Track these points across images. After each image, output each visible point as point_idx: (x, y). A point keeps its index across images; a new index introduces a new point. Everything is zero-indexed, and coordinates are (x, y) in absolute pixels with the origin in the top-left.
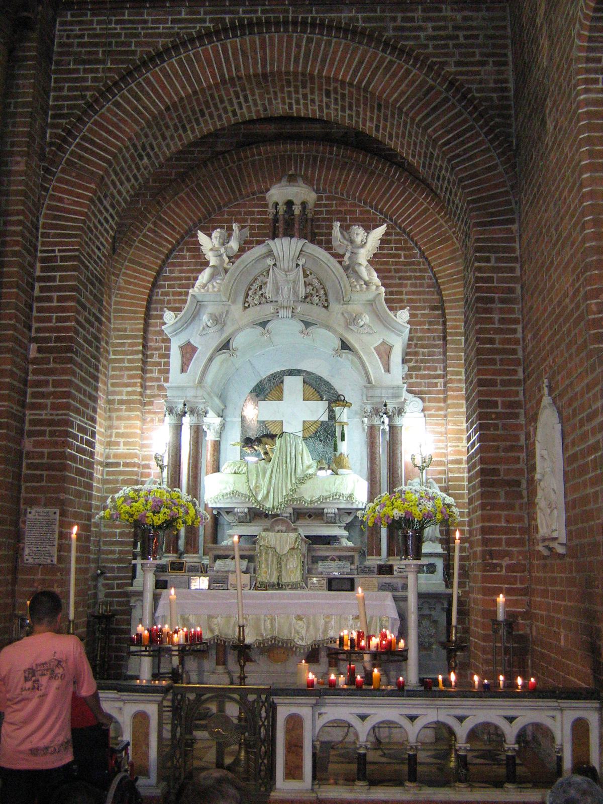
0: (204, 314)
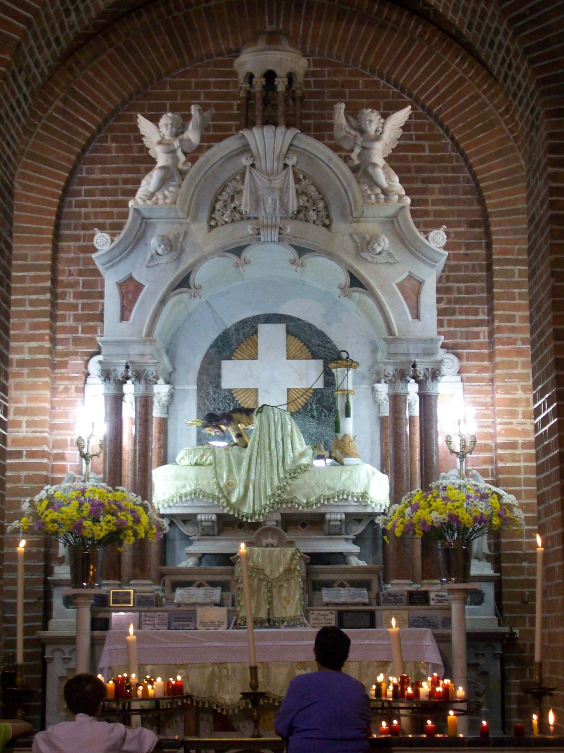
0: (152, 237)
